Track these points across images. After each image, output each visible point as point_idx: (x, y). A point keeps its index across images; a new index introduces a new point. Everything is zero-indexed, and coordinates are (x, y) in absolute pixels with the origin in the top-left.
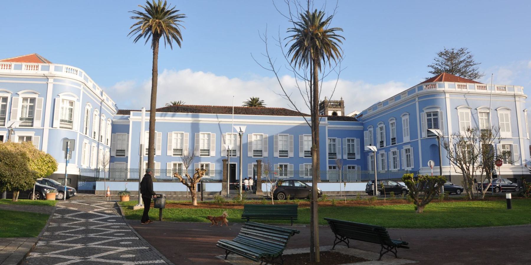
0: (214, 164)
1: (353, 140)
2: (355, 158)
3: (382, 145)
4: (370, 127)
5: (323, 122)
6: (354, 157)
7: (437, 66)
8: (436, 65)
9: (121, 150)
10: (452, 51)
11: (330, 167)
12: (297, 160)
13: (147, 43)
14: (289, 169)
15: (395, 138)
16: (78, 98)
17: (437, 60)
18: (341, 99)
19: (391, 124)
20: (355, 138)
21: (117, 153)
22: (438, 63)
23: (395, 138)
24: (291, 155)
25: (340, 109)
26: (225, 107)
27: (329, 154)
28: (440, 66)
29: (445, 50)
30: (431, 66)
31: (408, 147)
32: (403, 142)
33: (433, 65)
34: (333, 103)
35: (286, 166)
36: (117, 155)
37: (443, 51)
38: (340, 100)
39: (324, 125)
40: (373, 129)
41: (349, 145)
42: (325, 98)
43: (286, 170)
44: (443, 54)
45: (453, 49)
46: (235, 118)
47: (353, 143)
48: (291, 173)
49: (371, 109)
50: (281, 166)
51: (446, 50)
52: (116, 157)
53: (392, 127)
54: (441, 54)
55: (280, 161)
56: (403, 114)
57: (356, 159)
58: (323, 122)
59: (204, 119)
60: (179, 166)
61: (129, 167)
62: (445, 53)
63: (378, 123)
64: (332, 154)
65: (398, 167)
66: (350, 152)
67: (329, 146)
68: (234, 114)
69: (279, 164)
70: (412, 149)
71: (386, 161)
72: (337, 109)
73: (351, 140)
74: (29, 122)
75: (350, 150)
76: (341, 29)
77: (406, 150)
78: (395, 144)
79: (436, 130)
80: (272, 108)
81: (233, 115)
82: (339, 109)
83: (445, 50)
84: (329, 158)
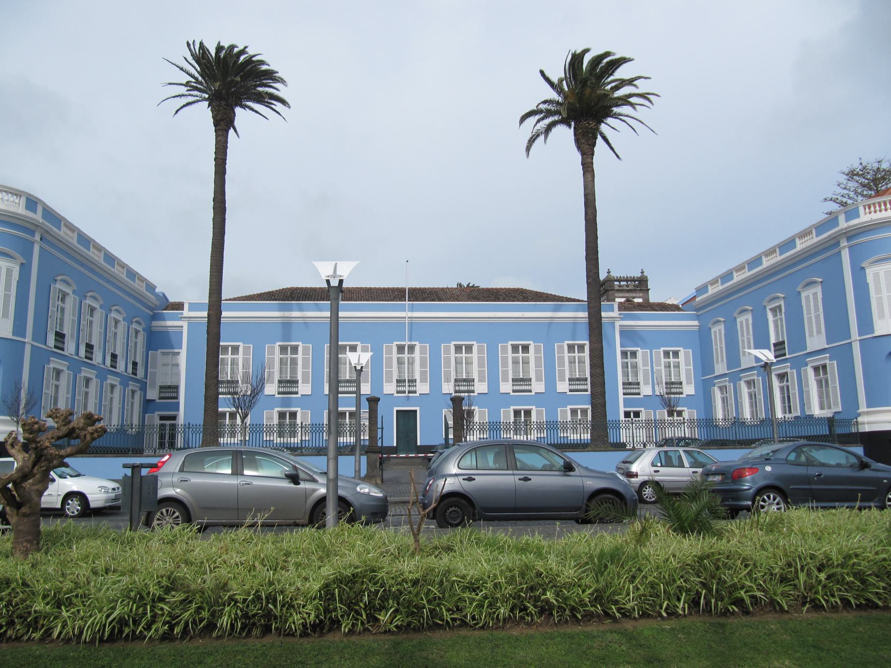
0: (543, 410)
1: (676, 353)
2: (639, 394)
3: (781, 352)
4: (745, 311)
5: (611, 314)
6: (528, 388)
7: (845, 200)
8: (842, 196)
9: (169, 387)
10: (876, 165)
11: (627, 414)
12: (550, 397)
13: (177, 114)
14: (534, 418)
15: (783, 342)
16: (24, 261)
17: (843, 186)
18: (642, 272)
19: (771, 309)
20: (681, 349)
21: (160, 392)
22: (846, 192)
23: (783, 342)
24: (538, 387)
25: (641, 294)
26: (393, 290)
27: (624, 384)
28: (850, 198)
29: (861, 164)
30: (831, 200)
31: (825, 359)
32: (873, 332)
33: (834, 197)
34: (625, 283)
35: (528, 413)
36: (161, 398)
37: (857, 167)
38: (639, 275)
39: (611, 320)
40: (723, 326)
41: (668, 366)
42: (609, 272)
43: (162, 437)
44: (857, 175)
45: (879, 162)
46: (412, 309)
47: (676, 360)
48: (540, 428)
49: (717, 281)
50: (517, 413)
51: (864, 164)
52: (158, 401)
53: (775, 316)
54: (852, 174)
55: (515, 401)
56: (804, 283)
57: (641, 396)
58: (611, 314)
59: (349, 313)
60: (290, 418)
61: (181, 420)
62: (861, 173)
63: (738, 311)
64: (630, 384)
65: (836, 404)
66: (671, 379)
67: (623, 367)
68: (408, 301)
69: (512, 408)
70: (833, 366)
71: (761, 397)
72: (634, 295)
73: (671, 353)
74: (353, 386)
75: (670, 376)
76: (607, 54)
77: (824, 367)
78: (785, 355)
79: (761, 350)
80: (496, 289)
81: (407, 302)
82: (638, 295)
83: (861, 164)
84: (624, 394)
